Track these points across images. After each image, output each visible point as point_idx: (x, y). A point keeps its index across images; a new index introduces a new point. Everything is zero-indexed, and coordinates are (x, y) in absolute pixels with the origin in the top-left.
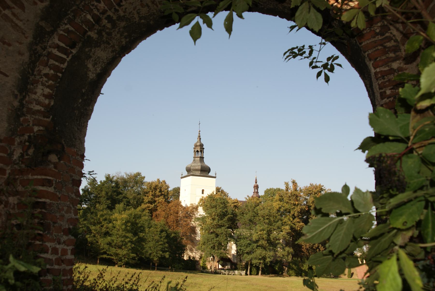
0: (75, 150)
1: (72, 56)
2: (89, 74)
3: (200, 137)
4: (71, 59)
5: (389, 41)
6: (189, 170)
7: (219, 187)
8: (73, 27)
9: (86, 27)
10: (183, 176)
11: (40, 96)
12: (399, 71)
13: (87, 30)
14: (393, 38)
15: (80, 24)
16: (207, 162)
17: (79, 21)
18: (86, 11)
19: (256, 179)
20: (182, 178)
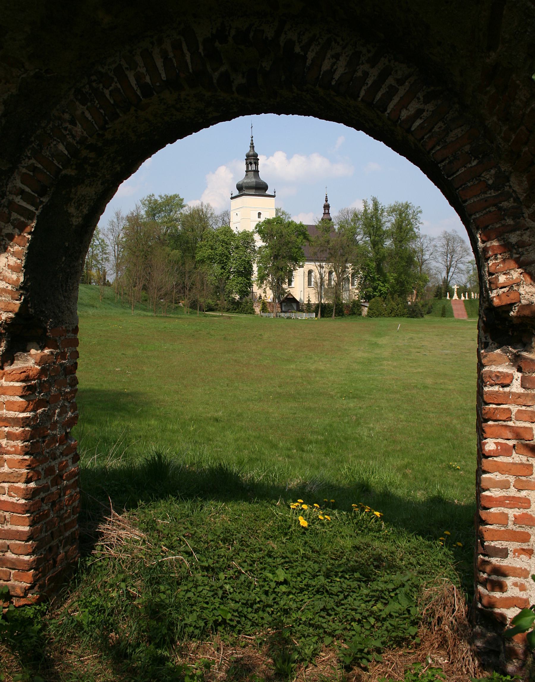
0: (64, 327)
1: (43, 207)
2: (72, 221)
3: (253, 144)
4: (42, 211)
5: (507, 200)
6: (240, 188)
8: (40, 163)
9: (58, 163)
10: (233, 196)
11: (4, 268)
12: (519, 247)
13: (61, 167)
14: (514, 195)
15: (50, 159)
16: (263, 176)
17: (48, 153)
18: (56, 138)
19: (326, 197)
20: (232, 198)
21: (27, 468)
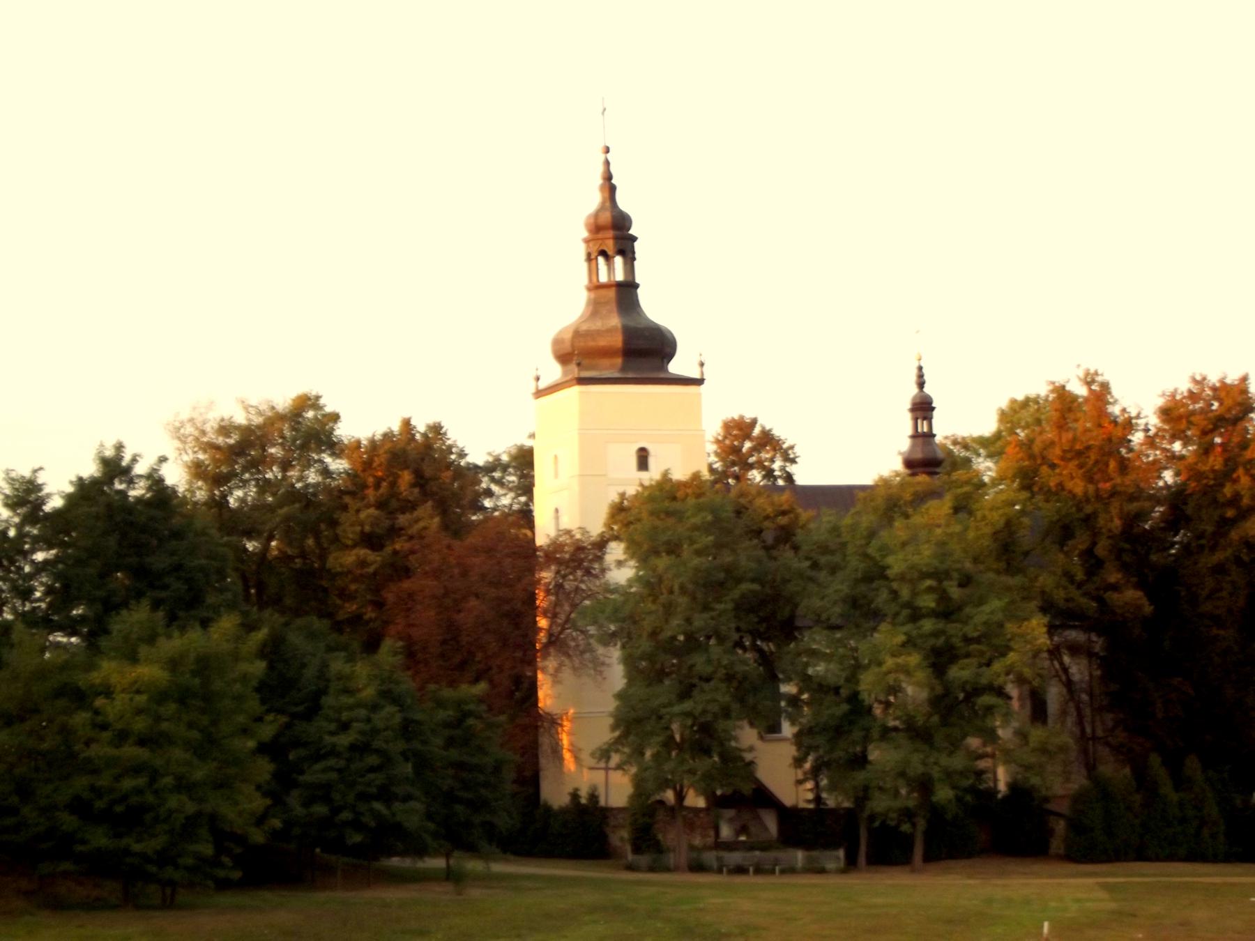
7: (748, 416)
10: (543, 384)
19: (920, 368)
20: (539, 393)
21: (10, 481)
